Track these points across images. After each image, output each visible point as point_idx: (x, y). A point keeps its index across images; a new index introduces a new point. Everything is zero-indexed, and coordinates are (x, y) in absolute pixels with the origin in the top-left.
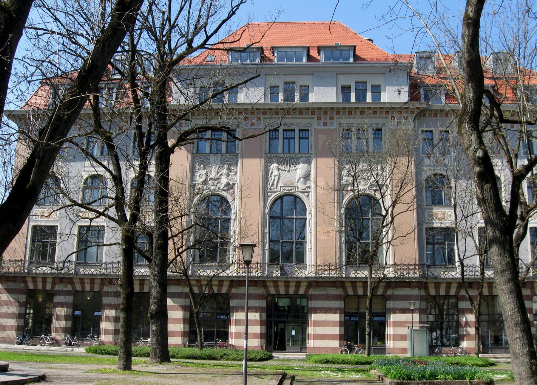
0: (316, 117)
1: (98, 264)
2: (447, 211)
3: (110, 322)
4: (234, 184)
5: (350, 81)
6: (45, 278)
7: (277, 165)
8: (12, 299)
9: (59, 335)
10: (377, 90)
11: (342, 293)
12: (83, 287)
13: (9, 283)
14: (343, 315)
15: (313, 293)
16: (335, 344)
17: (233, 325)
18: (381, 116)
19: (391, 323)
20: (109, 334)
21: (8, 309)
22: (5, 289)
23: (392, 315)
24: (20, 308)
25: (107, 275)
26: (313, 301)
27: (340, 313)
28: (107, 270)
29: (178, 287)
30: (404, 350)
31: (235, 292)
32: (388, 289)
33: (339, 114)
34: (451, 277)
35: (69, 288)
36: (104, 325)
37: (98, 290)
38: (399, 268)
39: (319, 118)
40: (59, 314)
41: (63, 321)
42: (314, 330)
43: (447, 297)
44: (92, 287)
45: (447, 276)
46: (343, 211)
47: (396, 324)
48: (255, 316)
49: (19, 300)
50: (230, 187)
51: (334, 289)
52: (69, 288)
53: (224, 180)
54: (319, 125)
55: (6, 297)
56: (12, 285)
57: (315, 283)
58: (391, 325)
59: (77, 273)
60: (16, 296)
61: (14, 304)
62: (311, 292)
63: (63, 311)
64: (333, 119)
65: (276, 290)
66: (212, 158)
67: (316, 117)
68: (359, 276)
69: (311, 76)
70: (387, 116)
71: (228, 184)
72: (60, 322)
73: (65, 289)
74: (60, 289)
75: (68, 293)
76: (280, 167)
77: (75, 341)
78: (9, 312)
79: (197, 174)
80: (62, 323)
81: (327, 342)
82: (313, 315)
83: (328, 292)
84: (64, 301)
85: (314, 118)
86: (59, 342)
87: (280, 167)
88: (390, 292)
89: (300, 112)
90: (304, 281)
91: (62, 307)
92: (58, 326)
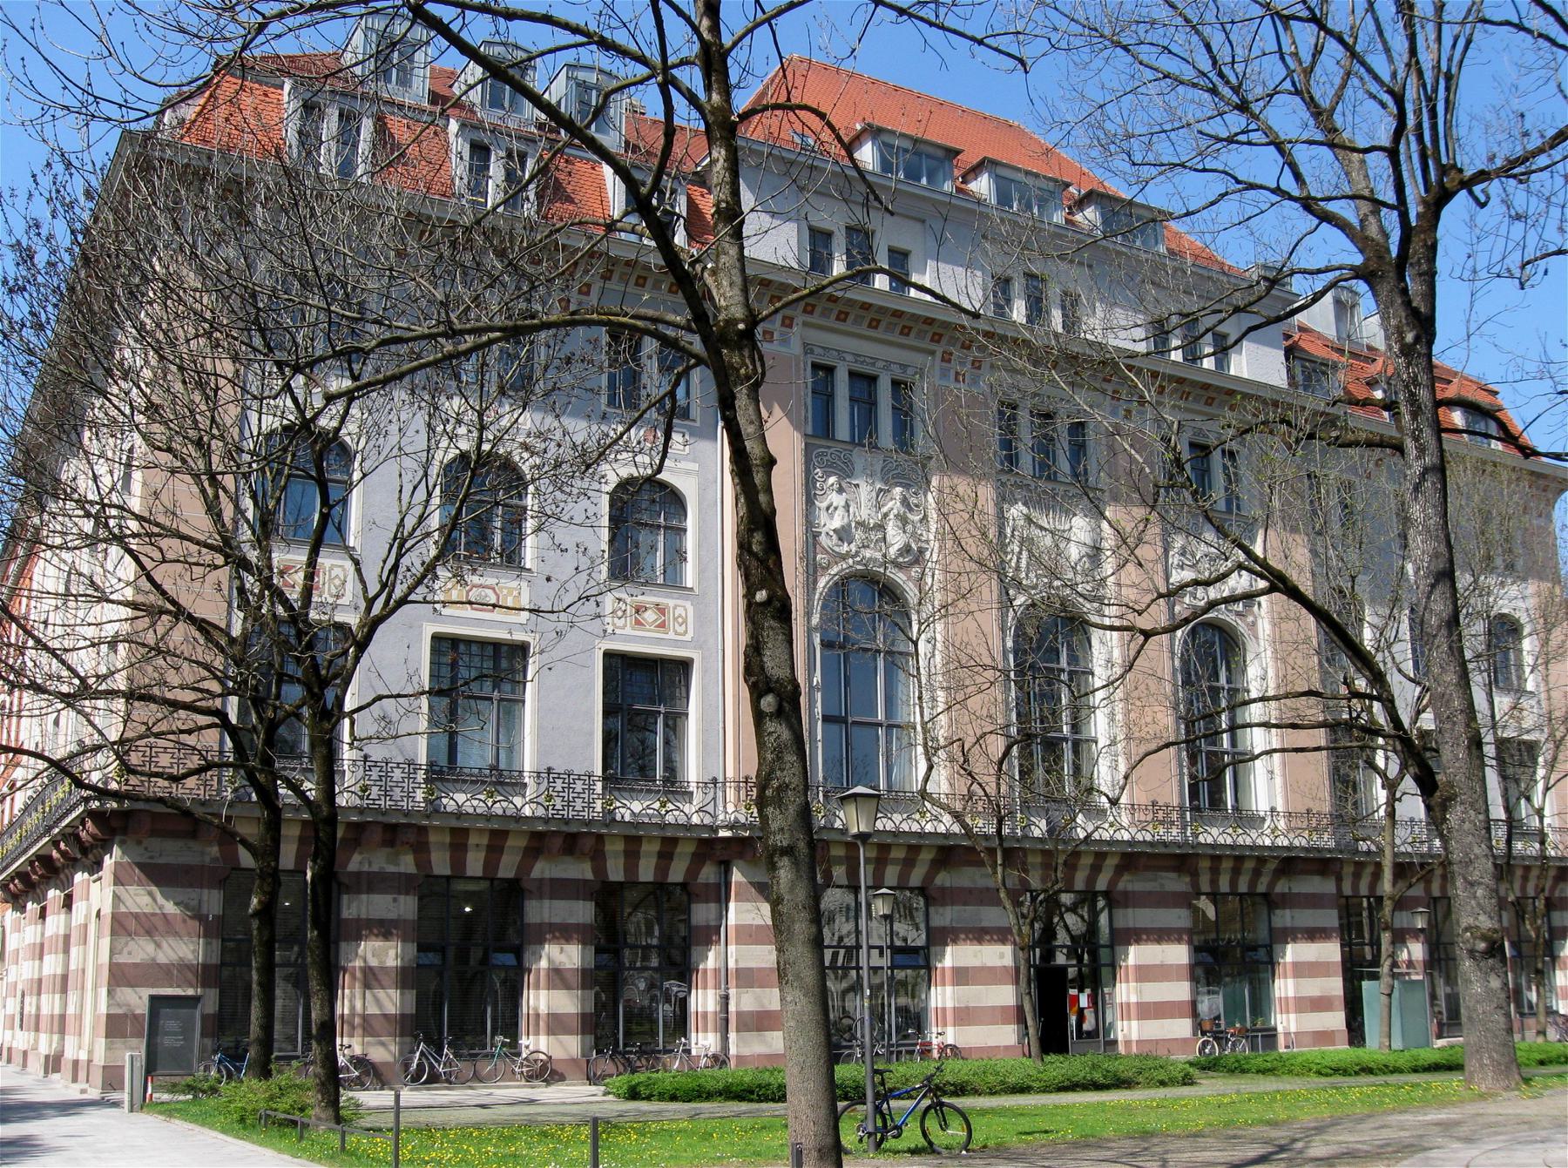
0: (939, 350)
1: (503, 779)
2: (671, 603)
3: (568, 987)
4: (921, 551)
5: (833, 218)
6: (465, 832)
7: (1025, 511)
8: (170, 908)
9: (383, 1044)
10: (1223, 350)
11: (589, 875)
12: (458, 862)
13: (155, 844)
14: (412, 949)
15: (1130, 888)
16: (1007, 1035)
17: (537, 987)
18: (822, 322)
19: (1289, 968)
20: (568, 1032)
21: (158, 946)
22: (141, 866)
23: (949, 949)
24: (207, 944)
25: (567, 821)
26: (1130, 911)
27: (584, 943)
28: (386, 793)
29: (1317, 879)
30: (1324, 1037)
31: (948, 884)
32: (536, 858)
33: (811, 313)
34: (682, 820)
35: (582, 870)
36: (538, 1000)
37: (511, 875)
38: (375, 774)
39: (946, 358)
40: (373, 962)
41: (392, 992)
42: (1140, 992)
43: (660, 888)
44: (491, 863)
45: (670, 818)
46: (1177, 663)
47: (962, 976)
48: (1002, 956)
49: (204, 911)
50: (913, 556)
51: (1173, 875)
52: (407, 864)
53: (896, 538)
54: (944, 374)
55: (147, 899)
56: (173, 852)
57: (1133, 859)
58: (1289, 972)
59: (433, 808)
60: (192, 894)
61: (179, 926)
62: (1127, 883)
63: (392, 953)
64: (790, 326)
65: (595, 871)
66: (860, 457)
67: (939, 350)
68: (1240, 841)
69: (918, 226)
70: (933, 347)
71: (906, 549)
72: (381, 993)
73: (391, 869)
74: (375, 868)
75: (400, 884)
76: (1035, 515)
77: (449, 1063)
78: (162, 959)
79: (821, 504)
80: (391, 1001)
81: (1167, 1022)
82: (1132, 949)
83: (1162, 885)
84: (392, 916)
85: (932, 353)
86: (383, 1070)
87: (1035, 515)
88: (1281, 887)
89: (875, 316)
90: (651, 839)
91: (386, 936)
92: (372, 1010)
